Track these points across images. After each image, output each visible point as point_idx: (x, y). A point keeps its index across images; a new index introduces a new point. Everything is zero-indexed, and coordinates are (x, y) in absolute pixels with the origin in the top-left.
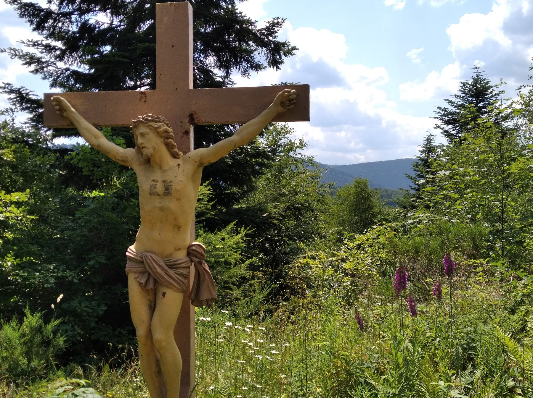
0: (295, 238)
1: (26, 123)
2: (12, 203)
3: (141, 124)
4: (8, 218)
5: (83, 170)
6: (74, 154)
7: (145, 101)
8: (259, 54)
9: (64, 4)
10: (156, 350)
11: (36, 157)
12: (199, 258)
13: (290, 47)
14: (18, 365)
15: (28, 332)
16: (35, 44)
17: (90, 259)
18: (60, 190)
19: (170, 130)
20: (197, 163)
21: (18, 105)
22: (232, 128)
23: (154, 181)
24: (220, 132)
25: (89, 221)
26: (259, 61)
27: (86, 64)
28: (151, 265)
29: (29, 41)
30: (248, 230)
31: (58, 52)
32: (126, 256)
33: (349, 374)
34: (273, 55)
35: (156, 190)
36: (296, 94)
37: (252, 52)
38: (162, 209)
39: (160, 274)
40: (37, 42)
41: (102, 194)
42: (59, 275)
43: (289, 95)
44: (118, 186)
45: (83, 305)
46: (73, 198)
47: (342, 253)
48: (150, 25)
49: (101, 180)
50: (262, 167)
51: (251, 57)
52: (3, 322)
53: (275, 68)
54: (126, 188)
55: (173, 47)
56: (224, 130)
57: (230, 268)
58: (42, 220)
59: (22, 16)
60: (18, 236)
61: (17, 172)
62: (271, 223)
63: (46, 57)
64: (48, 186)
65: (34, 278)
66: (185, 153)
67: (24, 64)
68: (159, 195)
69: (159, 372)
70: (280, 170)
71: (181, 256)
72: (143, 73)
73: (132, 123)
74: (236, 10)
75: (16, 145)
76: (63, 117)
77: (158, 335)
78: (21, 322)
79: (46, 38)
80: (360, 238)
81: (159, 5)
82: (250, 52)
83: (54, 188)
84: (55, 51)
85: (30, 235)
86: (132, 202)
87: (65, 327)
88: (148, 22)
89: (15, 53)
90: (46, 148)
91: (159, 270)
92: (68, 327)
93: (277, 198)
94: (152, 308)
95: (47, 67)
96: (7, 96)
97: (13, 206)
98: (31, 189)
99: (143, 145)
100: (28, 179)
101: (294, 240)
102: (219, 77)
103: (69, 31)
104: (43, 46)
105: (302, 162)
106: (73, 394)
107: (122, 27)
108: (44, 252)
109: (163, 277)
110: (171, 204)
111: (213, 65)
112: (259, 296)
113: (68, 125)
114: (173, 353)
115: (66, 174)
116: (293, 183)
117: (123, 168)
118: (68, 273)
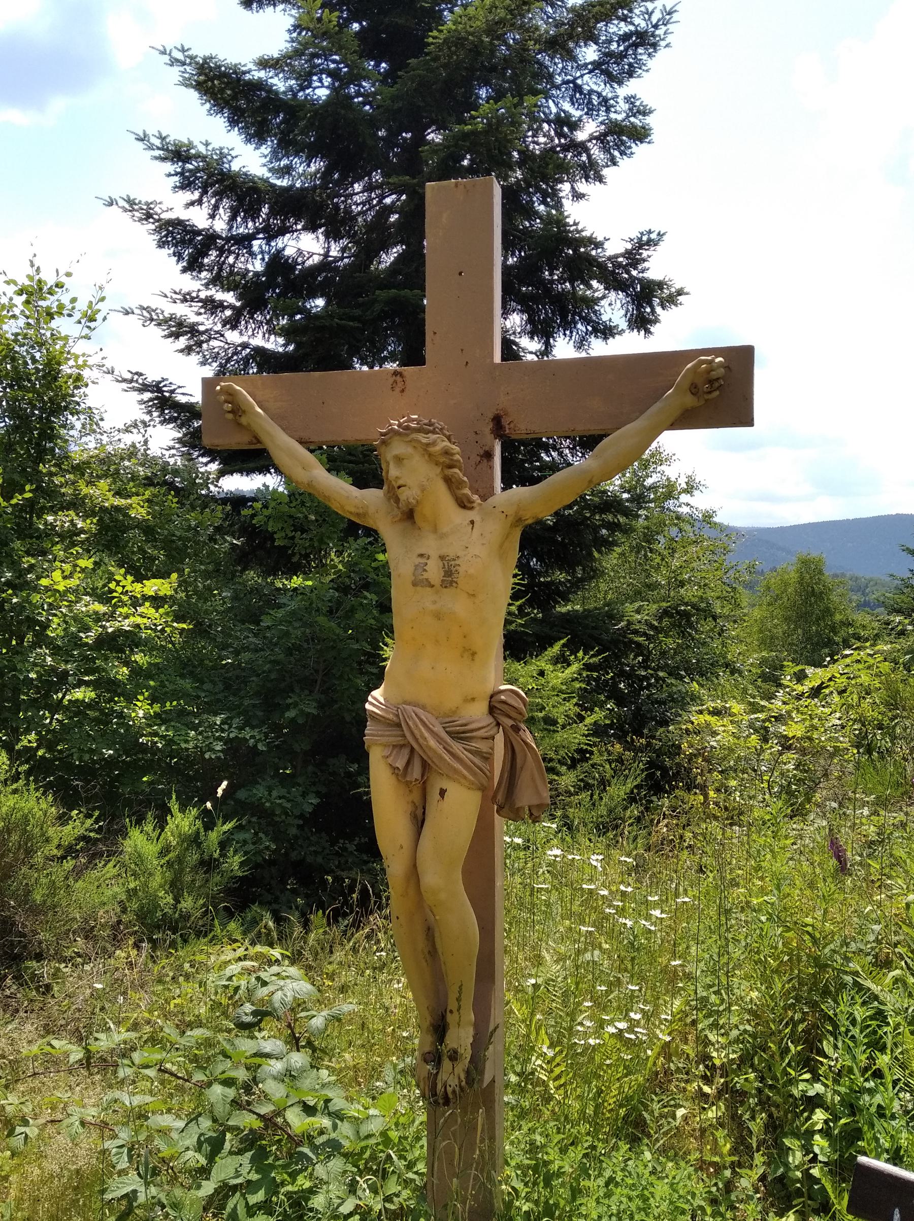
0: (683, 673)
1: (170, 448)
2: (145, 598)
3: (397, 438)
4: (138, 626)
5: (276, 536)
6: (258, 505)
7: (403, 391)
8: (610, 304)
9: (239, 219)
10: (428, 910)
11: (188, 512)
12: (514, 719)
13: (673, 290)
14: (157, 906)
15: (174, 843)
16: (187, 298)
17: (288, 707)
18: (234, 576)
19: (455, 448)
20: (510, 519)
21: (155, 414)
22: (554, 454)
23: (421, 555)
24: (531, 463)
25: (287, 634)
26: (610, 320)
27: (280, 335)
28: (416, 732)
29: (175, 293)
30: (593, 656)
31: (228, 313)
32: (365, 710)
33: (821, 965)
34: (639, 307)
35: (426, 575)
36: (726, 367)
37: (596, 301)
38: (438, 616)
39: (435, 752)
40: (189, 294)
41: (310, 583)
42: (232, 735)
43: (709, 371)
44: (340, 567)
45: (275, 793)
46: (256, 590)
47: (778, 705)
48: (400, 255)
49: (306, 556)
50: (613, 532)
51: (595, 312)
52: (128, 824)
53: (642, 332)
54: (353, 571)
55: (460, 274)
56: (540, 459)
57: (554, 731)
58: (201, 631)
59: (162, 244)
60: (158, 660)
61: (155, 540)
62: (631, 641)
63: (206, 322)
64: (210, 567)
65: (187, 741)
66: (484, 498)
67: (166, 337)
68: (433, 586)
69: (433, 953)
70: (649, 537)
71: (477, 713)
72: (385, 348)
73: (377, 436)
74: (568, 217)
75: (152, 489)
76: (239, 425)
77: (431, 878)
78: (161, 824)
79: (207, 286)
80: (816, 675)
81: (433, 187)
82: (592, 302)
83: (222, 572)
84: (222, 311)
85: (179, 658)
86: (366, 598)
87: (241, 836)
88: (395, 250)
89: (150, 316)
90: (207, 496)
91: (432, 743)
92: (247, 836)
93: (640, 593)
94: (419, 821)
95: (207, 341)
96: (135, 396)
97: (147, 604)
98: (181, 572)
99: (401, 482)
100: (174, 553)
101: (681, 678)
102: (531, 353)
103: (248, 271)
104: (201, 301)
105: (691, 520)
106: (258, 979)
107: (346, 260)
108: (204, 691)
109: (441, 758)
110: (457, 604)
111: (519, 330)
112: (618, 791)
113: (250, 443)
114: (459, 918)
115: (243, 544)
116: (676, 563)
117: (353, 529)
118: (247, 733)
